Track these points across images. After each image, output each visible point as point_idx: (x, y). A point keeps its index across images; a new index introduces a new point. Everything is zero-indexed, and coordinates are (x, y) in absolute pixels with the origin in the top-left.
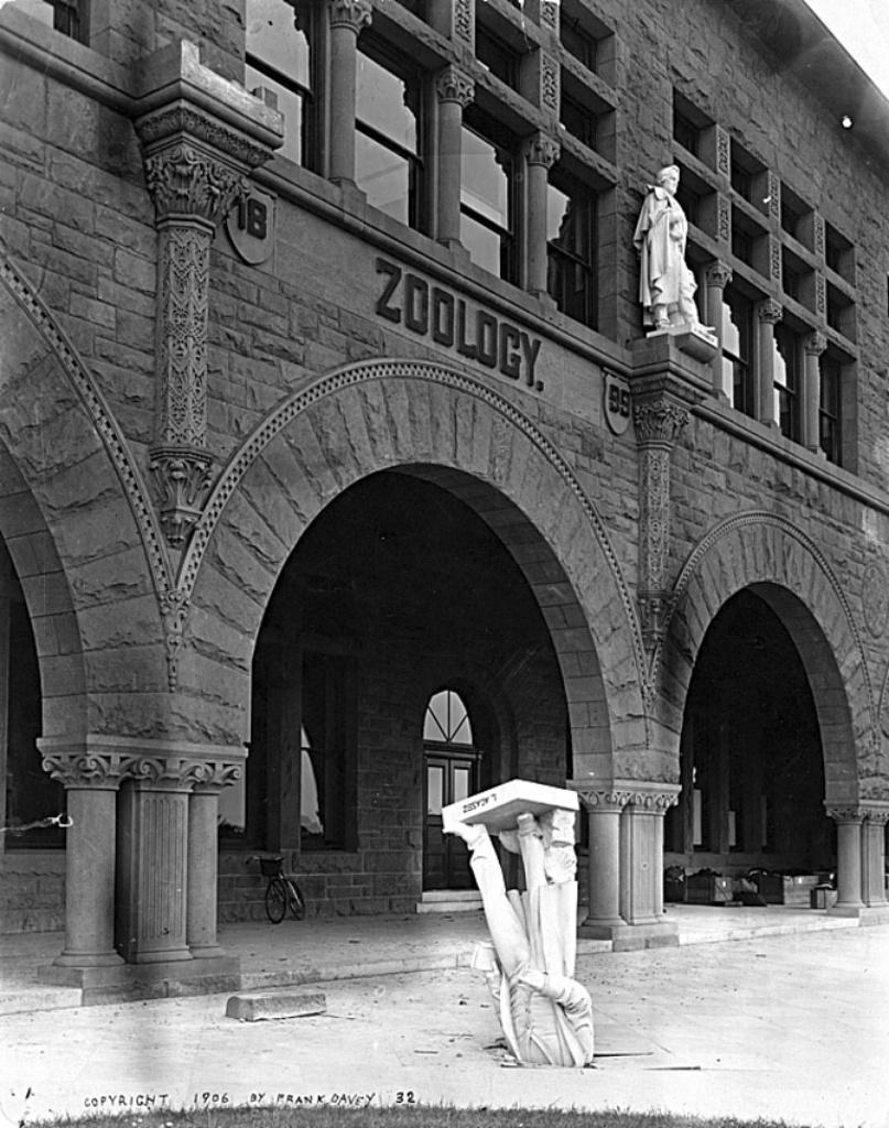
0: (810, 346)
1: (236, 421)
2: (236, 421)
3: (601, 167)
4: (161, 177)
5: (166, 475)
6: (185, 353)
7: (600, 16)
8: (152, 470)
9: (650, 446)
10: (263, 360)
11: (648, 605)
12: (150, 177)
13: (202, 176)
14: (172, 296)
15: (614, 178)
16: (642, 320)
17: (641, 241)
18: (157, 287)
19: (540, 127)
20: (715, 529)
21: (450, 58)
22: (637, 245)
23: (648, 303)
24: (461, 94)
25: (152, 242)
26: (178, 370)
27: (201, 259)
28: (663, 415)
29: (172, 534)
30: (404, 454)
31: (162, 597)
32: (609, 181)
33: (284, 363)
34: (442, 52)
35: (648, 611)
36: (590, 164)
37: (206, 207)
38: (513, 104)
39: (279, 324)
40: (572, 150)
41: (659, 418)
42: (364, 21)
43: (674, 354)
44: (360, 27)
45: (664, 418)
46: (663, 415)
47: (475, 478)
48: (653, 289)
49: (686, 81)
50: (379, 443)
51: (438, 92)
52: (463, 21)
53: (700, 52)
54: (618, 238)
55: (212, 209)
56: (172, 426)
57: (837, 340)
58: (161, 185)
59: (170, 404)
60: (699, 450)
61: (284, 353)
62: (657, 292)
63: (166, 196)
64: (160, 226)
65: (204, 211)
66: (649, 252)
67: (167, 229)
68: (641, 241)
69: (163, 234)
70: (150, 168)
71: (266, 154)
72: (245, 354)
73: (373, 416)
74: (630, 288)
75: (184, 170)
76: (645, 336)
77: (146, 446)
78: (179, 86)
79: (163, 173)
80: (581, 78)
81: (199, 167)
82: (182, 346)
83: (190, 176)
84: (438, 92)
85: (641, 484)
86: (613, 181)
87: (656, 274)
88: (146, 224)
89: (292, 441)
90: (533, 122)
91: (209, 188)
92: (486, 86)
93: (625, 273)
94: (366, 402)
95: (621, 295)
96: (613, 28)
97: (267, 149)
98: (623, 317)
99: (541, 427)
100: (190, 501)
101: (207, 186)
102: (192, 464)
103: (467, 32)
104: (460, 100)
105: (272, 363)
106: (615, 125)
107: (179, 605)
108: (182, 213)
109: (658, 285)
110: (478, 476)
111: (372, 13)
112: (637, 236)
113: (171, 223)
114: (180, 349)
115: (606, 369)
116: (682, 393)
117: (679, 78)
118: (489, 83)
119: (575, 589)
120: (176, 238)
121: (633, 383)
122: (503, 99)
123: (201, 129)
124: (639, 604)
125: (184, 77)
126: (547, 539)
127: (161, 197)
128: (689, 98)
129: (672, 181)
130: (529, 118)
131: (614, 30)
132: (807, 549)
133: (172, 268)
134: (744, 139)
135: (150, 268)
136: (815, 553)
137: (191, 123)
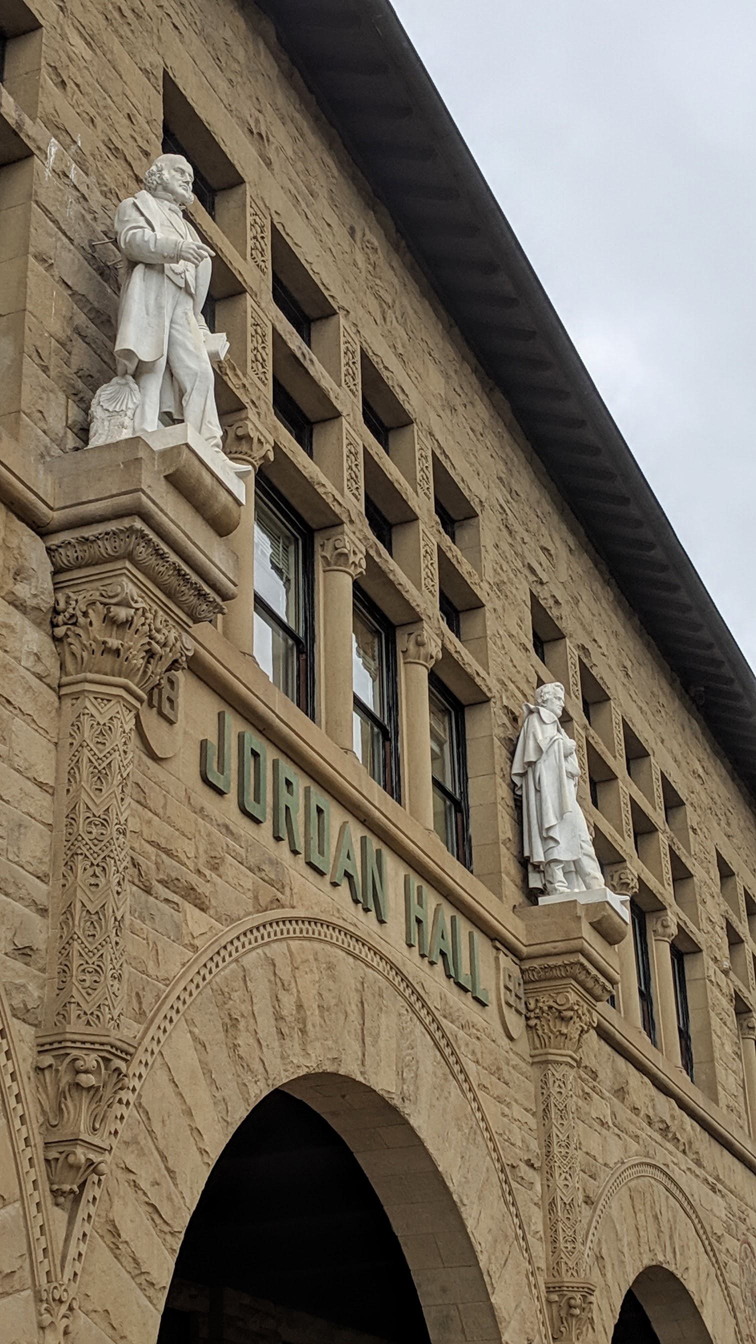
0: (660, 930)
1: (138, 994)
2: (138, 994)
3: (478, 674)
4: (82, 620)
5: (66, 1079)
6: (102, 881)
7: (466, 493)
8: (39, 1070)
9: (550, 1057)
10: (167, 900)
11: (563, 1303)
12: (60, 619)
13: (143, 625)
14: (84, 796)
15: (490, 690)
16: (525, 879)
17: (523, 775)
18: (56, 778)
19: (423, 617)
20: (610, 1184)
21: (344, 518)
22: (517, 780)
23: (539, 856)
24: (353, 563)
25: (53, 714)
26: (89, 907)
27: (125, 743)
28: (571, 1013)
29: (61, 1182)
30: (314, 1059)
31: (44, 1297)
32: (484, 694)
33: (188, 907)
34: (337, 509)
35: (563, 1314)
36: (469, 670)
37: (139, 669)
38: (400, 584)
39: (184, 847)
40: (452, 651)
41: (562, 1019)
42: (265, 457)
43: (587, 932)
44: (260, 463)
45: (571, 1018)
46: (571, 1013)
47: (382, 1098)
48: (547, 839)
49: (542, 583)
50: (288, 1039)
51: (324, 557)
52: (353, 476)
53: (548, 550)
54: (498, 770)
55: (145, 672)
56: (78, 998)
57: (685, 924)
58: (79, 631)
59: (76, 962)
60: (586, 1067)
61: (191, 894)
62: (552, 844)
63: (84, 647)
64: (64, 691)
65: (136, 674)
66: (538, 791)
67: (76, 696)
68: (523, 775)
69: (68, 702)
70: (62, 605)
71: (217, 606)
72: (148, 891)
73: (282, 995)
74: (514, 836)
75: (122, 613)
76: (536, 903)
77: (32, 1030)
78: (140, 499)
79: (85, 614)
80: (455, 563)
81: (141, 610)
82: (98, 871)
83: (129, 623)
84: (324, 557)
85: (541, 1113)
86: (489, 695)
87: (551, 819)
88: (49, 685)
89: (196, 1031)
90: (418, 609)
91: (149, 643)
92: (377, 559)
93: (507, 817)
94: (275, 974)
95: (504, 843)
96: (478, 510)
97: (218, 600)
98: (508, 874)
99: (445, 1023)
100: (97, 1126)
101: (148, 639)
102: (107, 1060)
103: (357, 488)
104: (351, 570)
105: (176, 906)
106: (485, 626)
107: (64, 1309)
108: (106, 674)
109: (554, 834)
110: (386, 1095)
111: (273, 448)
112: (517, 768)
113: (88, 687)
114: (95, 875)
115: (498, 945)
116: (590, 983)
117: (535, 579)
118: (380, 555)
119: (486, 1278)
120: (93, 711)
121: (526, 965)
122: (391, 577)
123: (153, 561)
124: (549, 1302)
125: (144, 487)
126: (455, 1197)
127: (76, 648)
128: (542, 602)
129: (557, 702)
130: (414, 604)
131: (479, 512)
132: (690, 1218)
133: (86, 753)
134: (590, 660)
135: (49, 751)
136: (696, 1221)
137: (142, 552)
